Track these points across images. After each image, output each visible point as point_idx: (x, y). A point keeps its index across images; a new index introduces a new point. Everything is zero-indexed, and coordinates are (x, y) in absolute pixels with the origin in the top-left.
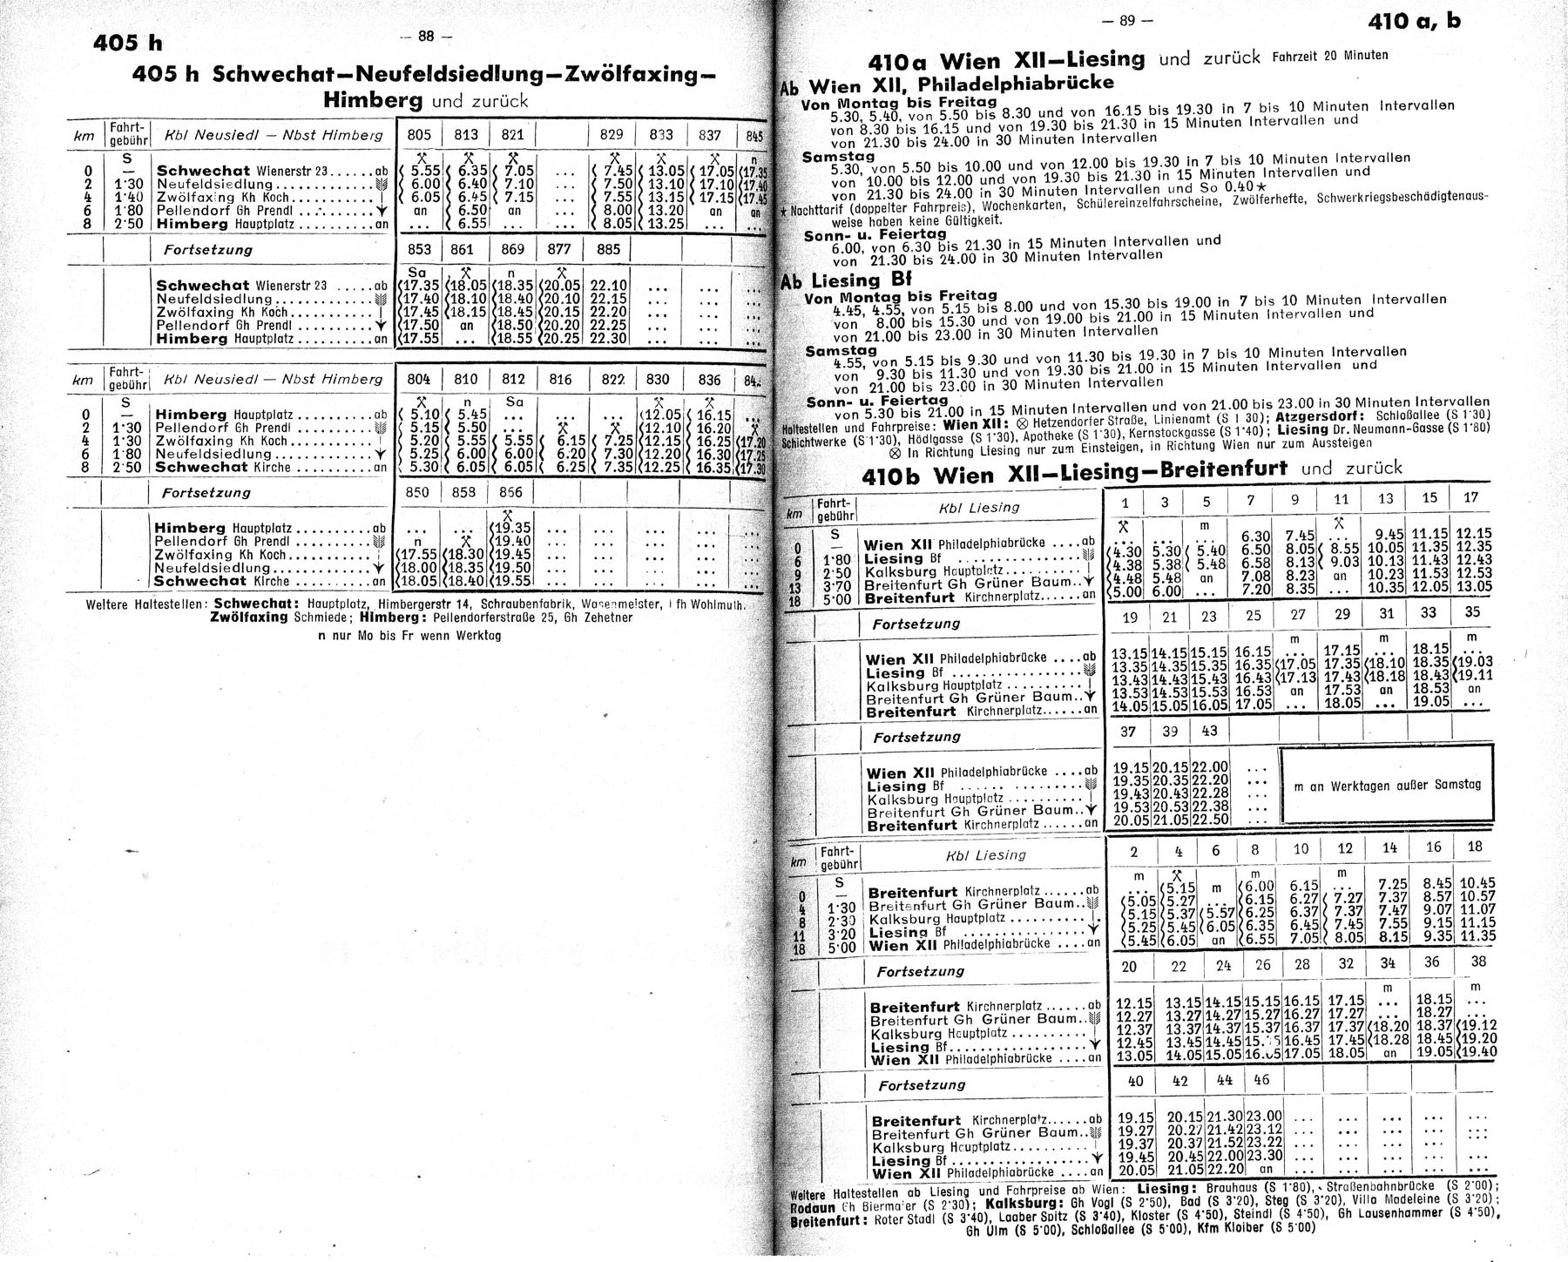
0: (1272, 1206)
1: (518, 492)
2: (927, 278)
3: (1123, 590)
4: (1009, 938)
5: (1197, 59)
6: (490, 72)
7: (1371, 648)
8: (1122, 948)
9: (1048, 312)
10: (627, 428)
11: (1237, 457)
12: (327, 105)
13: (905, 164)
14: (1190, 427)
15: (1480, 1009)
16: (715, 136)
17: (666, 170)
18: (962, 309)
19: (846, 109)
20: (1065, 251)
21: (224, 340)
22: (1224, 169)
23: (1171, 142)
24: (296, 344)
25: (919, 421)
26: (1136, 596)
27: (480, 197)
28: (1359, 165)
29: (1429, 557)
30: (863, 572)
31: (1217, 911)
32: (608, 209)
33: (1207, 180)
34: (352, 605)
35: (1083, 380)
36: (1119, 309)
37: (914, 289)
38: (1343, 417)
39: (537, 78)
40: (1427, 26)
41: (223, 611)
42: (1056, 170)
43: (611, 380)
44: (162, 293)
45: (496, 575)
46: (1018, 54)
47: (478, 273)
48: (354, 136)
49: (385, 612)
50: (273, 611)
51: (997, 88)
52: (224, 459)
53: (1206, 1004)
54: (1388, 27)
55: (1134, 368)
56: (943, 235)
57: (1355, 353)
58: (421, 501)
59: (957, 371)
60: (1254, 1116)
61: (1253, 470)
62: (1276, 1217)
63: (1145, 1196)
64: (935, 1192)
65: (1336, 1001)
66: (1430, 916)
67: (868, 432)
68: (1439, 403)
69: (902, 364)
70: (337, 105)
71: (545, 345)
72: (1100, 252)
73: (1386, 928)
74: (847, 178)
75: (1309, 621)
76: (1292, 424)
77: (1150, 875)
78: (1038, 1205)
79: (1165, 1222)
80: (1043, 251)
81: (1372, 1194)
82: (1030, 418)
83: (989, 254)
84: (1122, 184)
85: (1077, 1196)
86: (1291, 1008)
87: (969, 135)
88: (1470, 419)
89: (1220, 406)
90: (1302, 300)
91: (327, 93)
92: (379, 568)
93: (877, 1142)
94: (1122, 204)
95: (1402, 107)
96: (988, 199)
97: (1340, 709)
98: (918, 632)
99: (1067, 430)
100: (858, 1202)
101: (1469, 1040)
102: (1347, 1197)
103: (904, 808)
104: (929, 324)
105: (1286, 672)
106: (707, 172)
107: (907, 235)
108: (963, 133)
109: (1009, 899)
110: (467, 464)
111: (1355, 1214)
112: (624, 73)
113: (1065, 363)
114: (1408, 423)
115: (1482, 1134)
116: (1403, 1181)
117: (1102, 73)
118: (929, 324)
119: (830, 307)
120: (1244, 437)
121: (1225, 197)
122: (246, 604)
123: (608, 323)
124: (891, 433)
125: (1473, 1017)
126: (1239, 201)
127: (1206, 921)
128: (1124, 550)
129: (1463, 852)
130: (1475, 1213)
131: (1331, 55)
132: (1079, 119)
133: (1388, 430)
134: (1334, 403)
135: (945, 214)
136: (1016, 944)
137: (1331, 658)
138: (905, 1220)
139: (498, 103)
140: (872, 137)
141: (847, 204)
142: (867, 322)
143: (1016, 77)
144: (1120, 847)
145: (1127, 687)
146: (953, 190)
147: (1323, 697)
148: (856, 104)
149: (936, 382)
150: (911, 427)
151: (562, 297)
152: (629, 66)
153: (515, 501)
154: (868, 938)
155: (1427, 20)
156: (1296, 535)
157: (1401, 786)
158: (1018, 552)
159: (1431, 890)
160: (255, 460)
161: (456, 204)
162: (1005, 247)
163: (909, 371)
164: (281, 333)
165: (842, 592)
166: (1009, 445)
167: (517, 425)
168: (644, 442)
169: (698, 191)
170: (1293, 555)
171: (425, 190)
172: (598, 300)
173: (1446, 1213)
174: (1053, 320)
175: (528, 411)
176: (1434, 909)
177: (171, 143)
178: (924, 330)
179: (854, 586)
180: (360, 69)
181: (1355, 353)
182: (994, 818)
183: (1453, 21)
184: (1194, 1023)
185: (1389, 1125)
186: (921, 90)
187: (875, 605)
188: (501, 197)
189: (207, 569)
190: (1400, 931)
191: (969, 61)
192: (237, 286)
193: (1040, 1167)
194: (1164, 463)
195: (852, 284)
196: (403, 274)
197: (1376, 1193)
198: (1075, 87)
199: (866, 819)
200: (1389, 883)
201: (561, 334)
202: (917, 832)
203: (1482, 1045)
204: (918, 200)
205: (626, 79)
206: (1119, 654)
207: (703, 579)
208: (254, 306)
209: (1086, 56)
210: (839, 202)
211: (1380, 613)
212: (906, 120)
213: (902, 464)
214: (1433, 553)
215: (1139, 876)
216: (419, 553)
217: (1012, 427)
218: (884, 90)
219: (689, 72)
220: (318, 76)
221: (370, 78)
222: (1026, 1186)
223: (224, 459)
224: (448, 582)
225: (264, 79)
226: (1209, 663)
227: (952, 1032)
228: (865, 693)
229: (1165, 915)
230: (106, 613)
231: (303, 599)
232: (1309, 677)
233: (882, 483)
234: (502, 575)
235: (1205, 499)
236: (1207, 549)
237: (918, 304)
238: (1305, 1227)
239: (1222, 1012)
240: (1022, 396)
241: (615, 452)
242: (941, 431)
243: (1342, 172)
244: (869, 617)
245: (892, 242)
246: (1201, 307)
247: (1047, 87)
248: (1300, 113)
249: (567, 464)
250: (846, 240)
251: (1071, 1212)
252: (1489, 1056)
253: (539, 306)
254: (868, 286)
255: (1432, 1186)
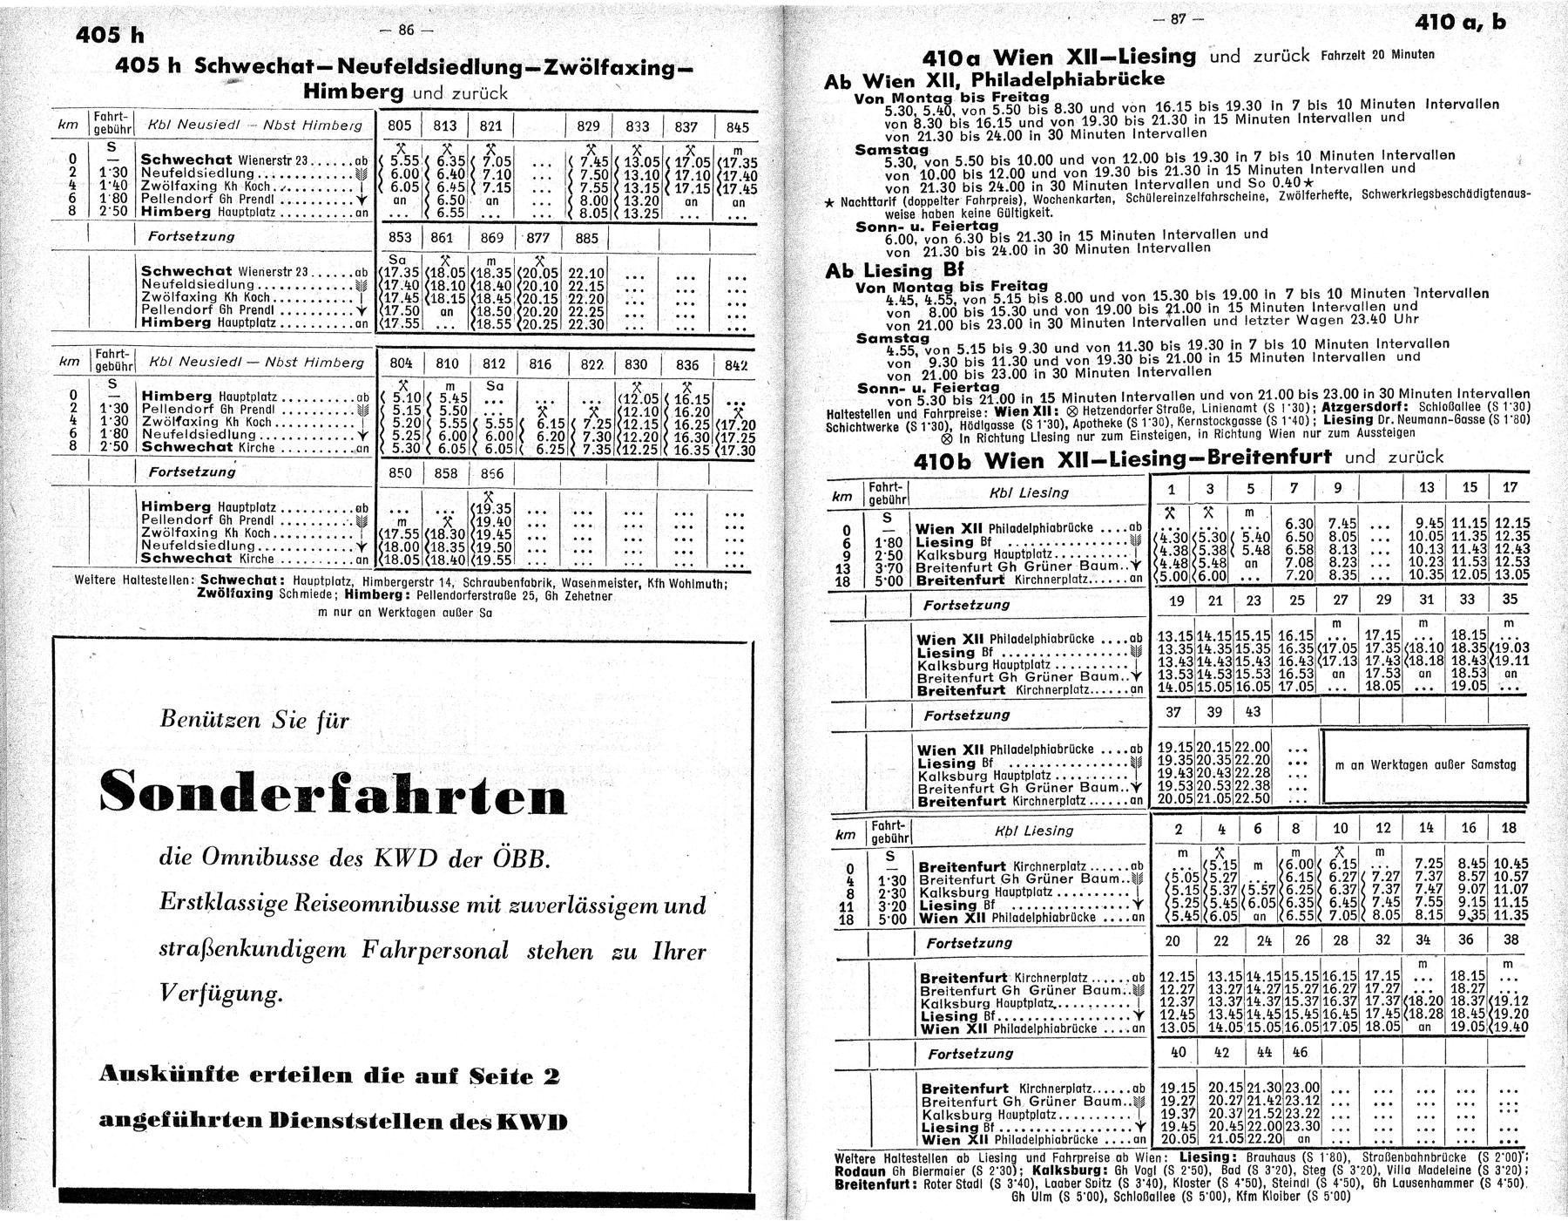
0: (1309, 1176)
1: (500, 475)
2: (980, 269)
3: (1169, 573)
4: (1056, 912)
5: (1247, 57)
6: (470, 65)
7: (1411, 633)
8: (1166, 923)
9: (1098, 303)
10: (606, 412)
11: (1284, 446)
12: (307, 96)
13: (958, 158)
14: (1238, 416)
15: (1512, 986)
16: (691, 127)
17: (641, 162)
18: (1014, 299)
19: (900, 103)
20: (1115, 243)
21: (207, 324)
22: (1272, 165)
23: (1223, 137)
24: (278, 328)
25: (971, 408)
26: (1180, 578)
27: (458, 188)
28: (1404, 160)
29: (1469, 546)
30: (915, 555)
31: (1258, 888)
32: (584, 200)
33: (1255, 176)
34: (339, 582)
35: (1132, 369)
36: (1168, 301)
37: (966, 279)
38: (1387, 408)
39: (516, 71)
40: (1473, 27)
41: (209, 587)
42: (1107, 164)
43: (590, 366)
44: (147, 278)
45: (477, 555)
46: (1071, 51)
47: (457, 261)
48: (334, 126)
49: (370, 589)
50: (259, 587)
51: (1049, 84)
52: (210, 439)
53: (1247, 978)
54: (1435, 27)
55: (1183, 357)
56: (995, 227)
57: (1399, 345)
58: (404, 481)
59: (1009, 359)
60: (1293, 1088)
61: (1297, 459)
62: (1313, 1186)
63: (1187, 1164)
64: (983, 1159)
65: (1372, 976)
66: (1465, 894)
67: (920, 419)
68: (1480, 394)
69: (954, 352)
70: (316, 96)
71: (524, 331)
72: (1149, 245)
73: (1421, 907)
74: (901, 171)
75: (1351, 606)
76: (1338, 415)
77: (1193, 851)
78: (1083, 1171)
79: (1205, 1190)
80: (1093, 244)
81: (1406, 1165)
82: (1080, 406)
83: (1040, 245)
84: (1172, 179)
85: (1121, 1164)
86: (1330, 983)
87: (1022, 129)
88: (1510, 411)
89: (1266, 396)
90: (1347, 293)
91: (307, 85)
92: (362, 547)
93: (927, 1109)
94: (1170, 198)
95: (1448, 105)
96: (1040, 193)
97: (1380, 692)
98: (969, 613)
99: (1116, 417)
100: (908, 1167)
101: (1501, 1016)
102: (1382, 1167)
103: (954, 784)
104: (981, 313)
105: (1328, 655)
106: (682, 163)
107: (960, 227)
108: (1015, 127)
109: (1058, 873)
110: (448, 445)
111: (1390, 1183)
112: (602, 66)
113: (1114, 352)
114: (1450, 415)
115: (1512, 1108)
116: (1436, 1152)
117: (1152, 69)
118: (981, 313)
119: (882, 297)
120: (1290, 426)
121: (1271, 192)
122: (232, 581)
123: (586, 311)
124: (943, 420)
125: (1505, 993)
126: (1285, 197)
127: (1248, 897)
128: (1170, 536)
129: (1497, 833)
130: (1505, 1183)
131: (1379, 54)
132: (1130, 115)
133: (1431, 420)
134: (1378, 393)
135: (997, 206)
136: (1061, 918)
137: (1372, 642)
138: (953, 1185)
139: (477, 95)
140: (925, 131)
141: (900, 197)
142: (920, 311)
143: (1068, 73)
144: (1164, 825)
145: (1172, 668)
146: (1006, 183)
147: (1364, 680)
148: (911, 99)
149: (987, 370)
150: (963, 414)
151: (541, 286)
152: (607, 60)
153: (497, 482)
154: (918, 910)
155: (1473, 21)
156: (1338, 523)
157: (1438, 766)
158: (1066, 536)
159: (1465, 870)
160: (240, 440)
161: (435, 194)
162: (1056, 239)
163: (961, 359)
164: (263, 317)
165: (895, 573)
166: (1058, 431)
167: (497, 408)
168: (623, 425)
169: (673, 181)
170: (1336, 542)
171: (404, 180)
172: (576, 287)
173: (1476, 1184)
174: (1103, 311)
175: (508, 394)
176: (1468, 888)
177: (154, 133)
178: (974, 319)
179: (906, 568)
180: (341, 61)
181: (1399, 345)
182: (1041, 795)
183: (1499, 23)
184: (1235, 996)
185: (1423, 1098)
186: (974, 85)
187: (926, 587)
188: (479, 188)
189: (192, 546)
190: (1435, 909)
191: (1022, 57)
192: (220, 272)
193: (1084, 1135)
194: (1210, 451)
195: (905, 275)
196: (384, 261)
197: (1410, 1164)
198: (1127, 83)
199: (917, 795)
200: (1425, 863)
201: (540, 321)
202: (967, 808)
203: (1514, 1020)
204: (970, 193)
205: (604, 73)
206: (1165, 636)
207: (680, 559)
208: (236, 291)
209: (1137, 53)
210: (892, 194)
211: (1421, 599)
212: (959, 114)
213: (954, 449)
214: (1473, 542)
215: (1182, 853)
216: (402, 532)
217: (1063, 414)
218: (938, 85)
219: (1187, 53)
220: (298, 68)
221: (351, 70)
222: (1072, 1153)
223: (210, 439)
224: (430, 561)
225: (245, 70)
226: (1253, 646)
227: (999, 1002)
228: (916, 672)
229: (1208, 891)
230: (94, 587)
231: (288, 577)
232: (1350, 661)
233: (934, 467)
234: (483, 555)
235: (1250, 486)
236: (1252, 535)
237: (969, 294)
238: (1339, 1196)
239: (1263, 986)
240: (1072, 384)
241: (594, 435)
242: (992, 417)
243: (1388, 169)
244: (920, 598)
245: (944, 234)
246: (1245, 299)
247: (1099, 83)
248: (1350, 112)
249: (546, 446)
250: (899, 232)
251: (1114, 1179)
252: (1521, 1031)
253: (517, 293)
254: (921, 276)
255: (1464, 1158)
